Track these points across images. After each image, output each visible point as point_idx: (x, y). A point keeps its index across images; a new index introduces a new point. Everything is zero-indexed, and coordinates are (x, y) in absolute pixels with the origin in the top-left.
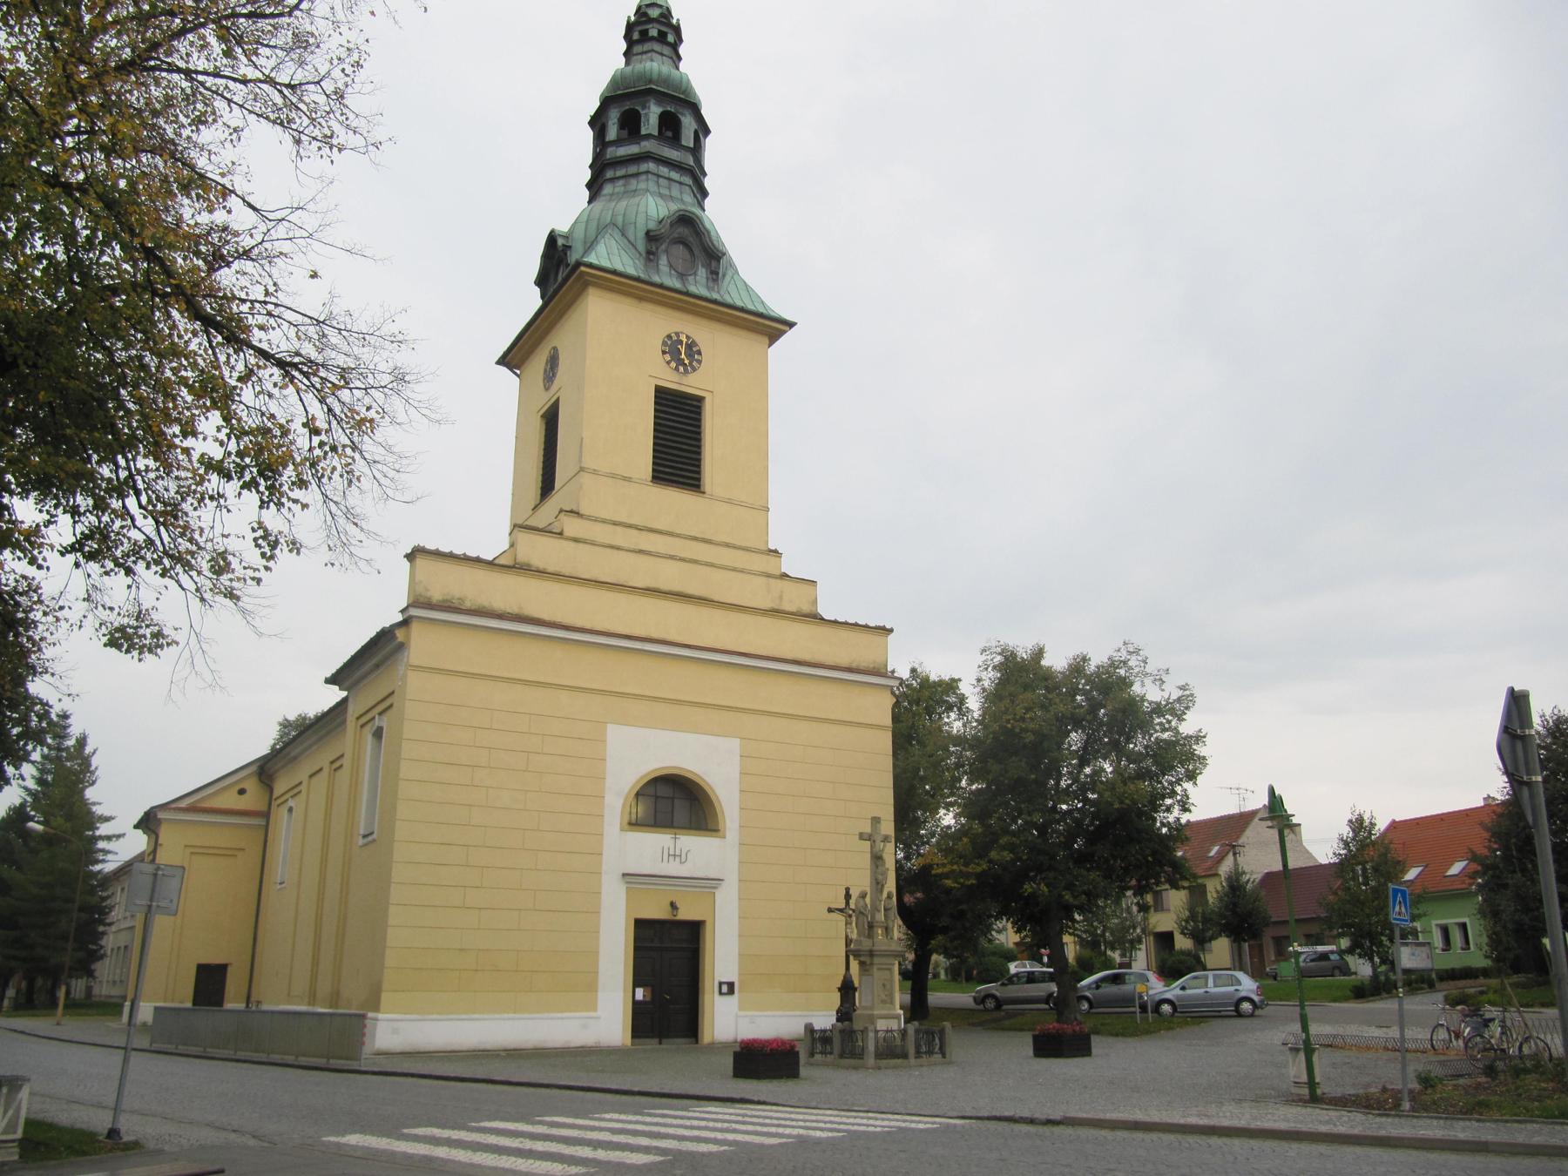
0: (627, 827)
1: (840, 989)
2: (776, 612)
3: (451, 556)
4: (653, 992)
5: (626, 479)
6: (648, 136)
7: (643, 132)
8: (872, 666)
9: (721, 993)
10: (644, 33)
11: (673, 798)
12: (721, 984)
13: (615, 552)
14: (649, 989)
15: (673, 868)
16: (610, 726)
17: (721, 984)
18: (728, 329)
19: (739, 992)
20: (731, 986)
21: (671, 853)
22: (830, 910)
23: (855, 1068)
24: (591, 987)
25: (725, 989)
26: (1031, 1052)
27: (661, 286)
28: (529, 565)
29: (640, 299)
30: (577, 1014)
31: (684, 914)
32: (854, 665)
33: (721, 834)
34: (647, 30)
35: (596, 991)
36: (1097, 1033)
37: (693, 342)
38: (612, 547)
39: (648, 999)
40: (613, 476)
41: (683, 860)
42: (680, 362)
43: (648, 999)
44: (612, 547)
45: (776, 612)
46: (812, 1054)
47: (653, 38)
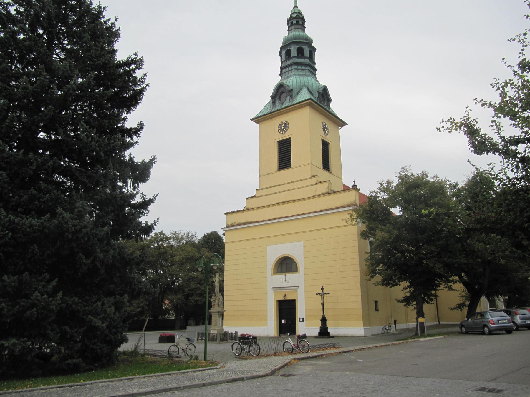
0: (273, 274)
1: (321, 320)
2: (314, 197)
3: (234, 212)
4: (287, 321)
5: (270, 174)
6: (294, 57)
7: (292, 56)
8: (349, 203)
9: (300, 321)
10: (292, 23)
11: (287, 263)
12: (300, 318)
13: (268, 196)
14: (285, 320)
15: (285, 285)
16: (268, 246)
17: (300, 318)
18: (296, 111)
19: (306, 321)
20: (303, 319)
21: (285, 280)
22: (317, 294)
23: (227, 343)
24: (266, 320)
25: (301, 320)
26: (158, 341)
27: (278, 110)
28: (249, 208)
29: (271, 118)
30: (262, 327)
31: (289, 298)
32: (342, 205)
33: (298, 272)
34: (293, 22)
35: (267, 321)
36: (273, 338)
37: (287, 122)
38: (267, 195)
39: (285, 323)
40: (267, 174)
41: (288, 281)
42: (283, 130)
43: (285, 323)
44: (267, 195)
45: (314, 197)
46: (198, 340)
47: (295, 24)
